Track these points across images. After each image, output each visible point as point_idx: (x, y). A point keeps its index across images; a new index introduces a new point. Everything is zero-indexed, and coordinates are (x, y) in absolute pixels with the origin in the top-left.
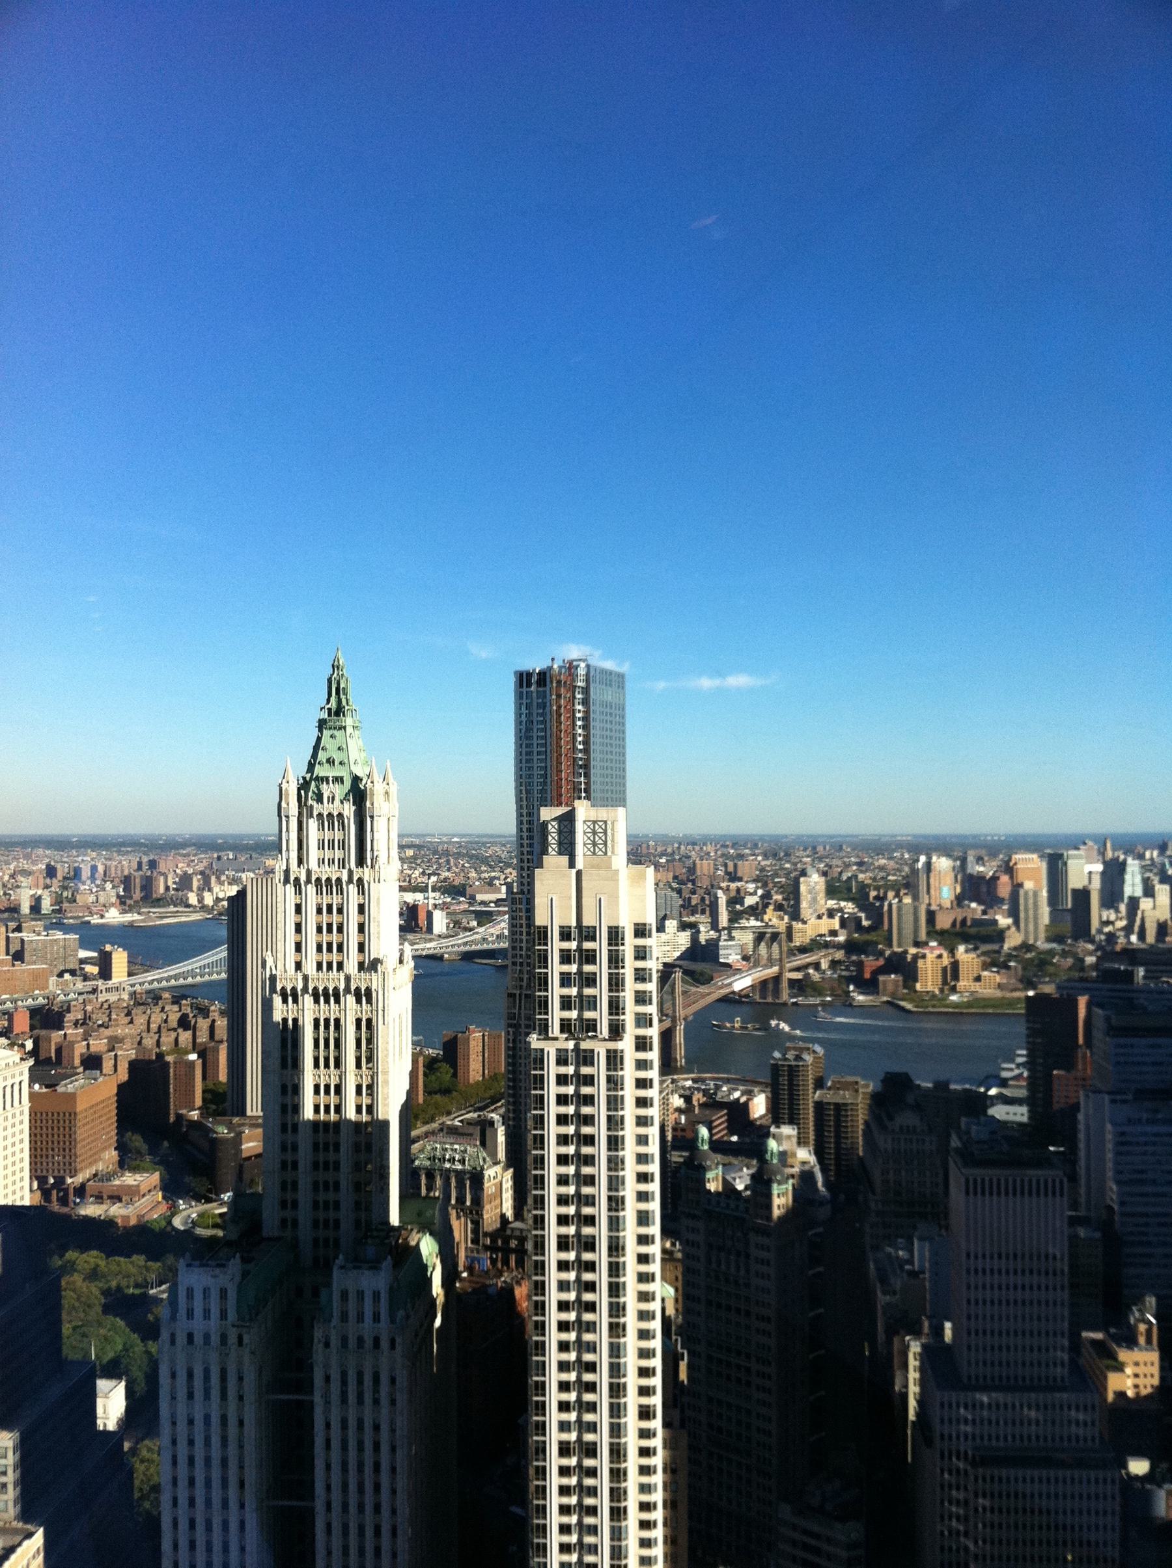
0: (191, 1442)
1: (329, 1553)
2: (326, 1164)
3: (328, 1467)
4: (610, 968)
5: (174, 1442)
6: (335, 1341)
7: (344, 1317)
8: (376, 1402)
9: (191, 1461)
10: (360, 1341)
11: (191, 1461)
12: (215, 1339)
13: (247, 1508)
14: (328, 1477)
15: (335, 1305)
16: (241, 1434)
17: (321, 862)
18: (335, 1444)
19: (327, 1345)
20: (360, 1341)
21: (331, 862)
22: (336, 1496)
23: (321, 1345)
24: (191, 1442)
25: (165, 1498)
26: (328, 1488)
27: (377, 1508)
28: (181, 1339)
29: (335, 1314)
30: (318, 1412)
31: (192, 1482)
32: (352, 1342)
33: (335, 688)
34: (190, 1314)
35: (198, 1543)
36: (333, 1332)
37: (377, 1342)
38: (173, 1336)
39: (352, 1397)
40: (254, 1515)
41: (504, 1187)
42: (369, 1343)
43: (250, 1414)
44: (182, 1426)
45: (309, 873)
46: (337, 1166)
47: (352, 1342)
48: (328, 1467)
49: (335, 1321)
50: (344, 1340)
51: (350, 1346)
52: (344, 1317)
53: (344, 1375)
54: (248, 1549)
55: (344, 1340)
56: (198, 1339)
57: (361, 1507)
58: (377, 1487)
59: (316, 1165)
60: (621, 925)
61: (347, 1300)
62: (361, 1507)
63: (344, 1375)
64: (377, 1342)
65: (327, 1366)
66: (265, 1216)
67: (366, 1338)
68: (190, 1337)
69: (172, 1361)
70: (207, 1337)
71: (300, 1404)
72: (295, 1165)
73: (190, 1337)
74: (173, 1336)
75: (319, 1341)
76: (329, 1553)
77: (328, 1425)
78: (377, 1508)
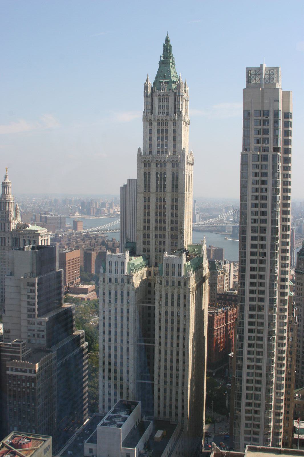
0: (110, 318)
1: (160, 361)
2: (160, 227)
3: (160, 328)
4: (272, 202)
5: (104, 318)
6: (164, 283)
7: (167, 274)
8: (179, 305)
9: (110, 325)
10: (173, 282)
11: (110, 325)
12: (119, 281)
13: (130, 343)
14: (159, 357)
15: (164, 269)
16: (128, 362)
17: (159, 113)
18: (163, 329)
19: (161, 284)
20: (173, 282)
21: (163, 113)
22: (163, 325)
23: (158, 284)
24: (110, 318)
25: (100, 331)
26: (160, 337)
27: (178, 345)
28: (107, 280)
29: (164, 273)
30: (157, 308)
31: (110, 332)
32: (170, 283)
33: (167, 49)
34: (110, 272)
35: (112, 324)
36: (163, 279)
37: (179, 283)
38: (104, 279)
39: (170, 304)
40: (133, 309)
41: (225, 278)
42: (176, 283)
43: (132, 309)
44: (107, 313)
45: (153, 157)
46: (164, 229)
47: (170, 283)
48: (160, 328)
49: (164, 275)
50: (167, 282)
51: (169, 284)
52: (167, 274)
53: (167, 295)
54: (130, 358)
55: (167, 282)
56: (113, 280)
57: (172, 344)
58: (178, 337)
59: (156, 229)
60: (290, 112)
61: (168, 268)
62: (172, 344)
63: (167, 295)
64: (179, 283)
65: (160, 292)
66: (137, 247)
67: (175, 282)
68: (110, 280)
69: (104, 289)
70: (116, 280)
71: (149, 308)
72: (149, 228)
73: (110, 280)
74: (104, 279)
75: (158, 282)
76: (160, 361)
77: (160, 314)
78: (178, 345)
